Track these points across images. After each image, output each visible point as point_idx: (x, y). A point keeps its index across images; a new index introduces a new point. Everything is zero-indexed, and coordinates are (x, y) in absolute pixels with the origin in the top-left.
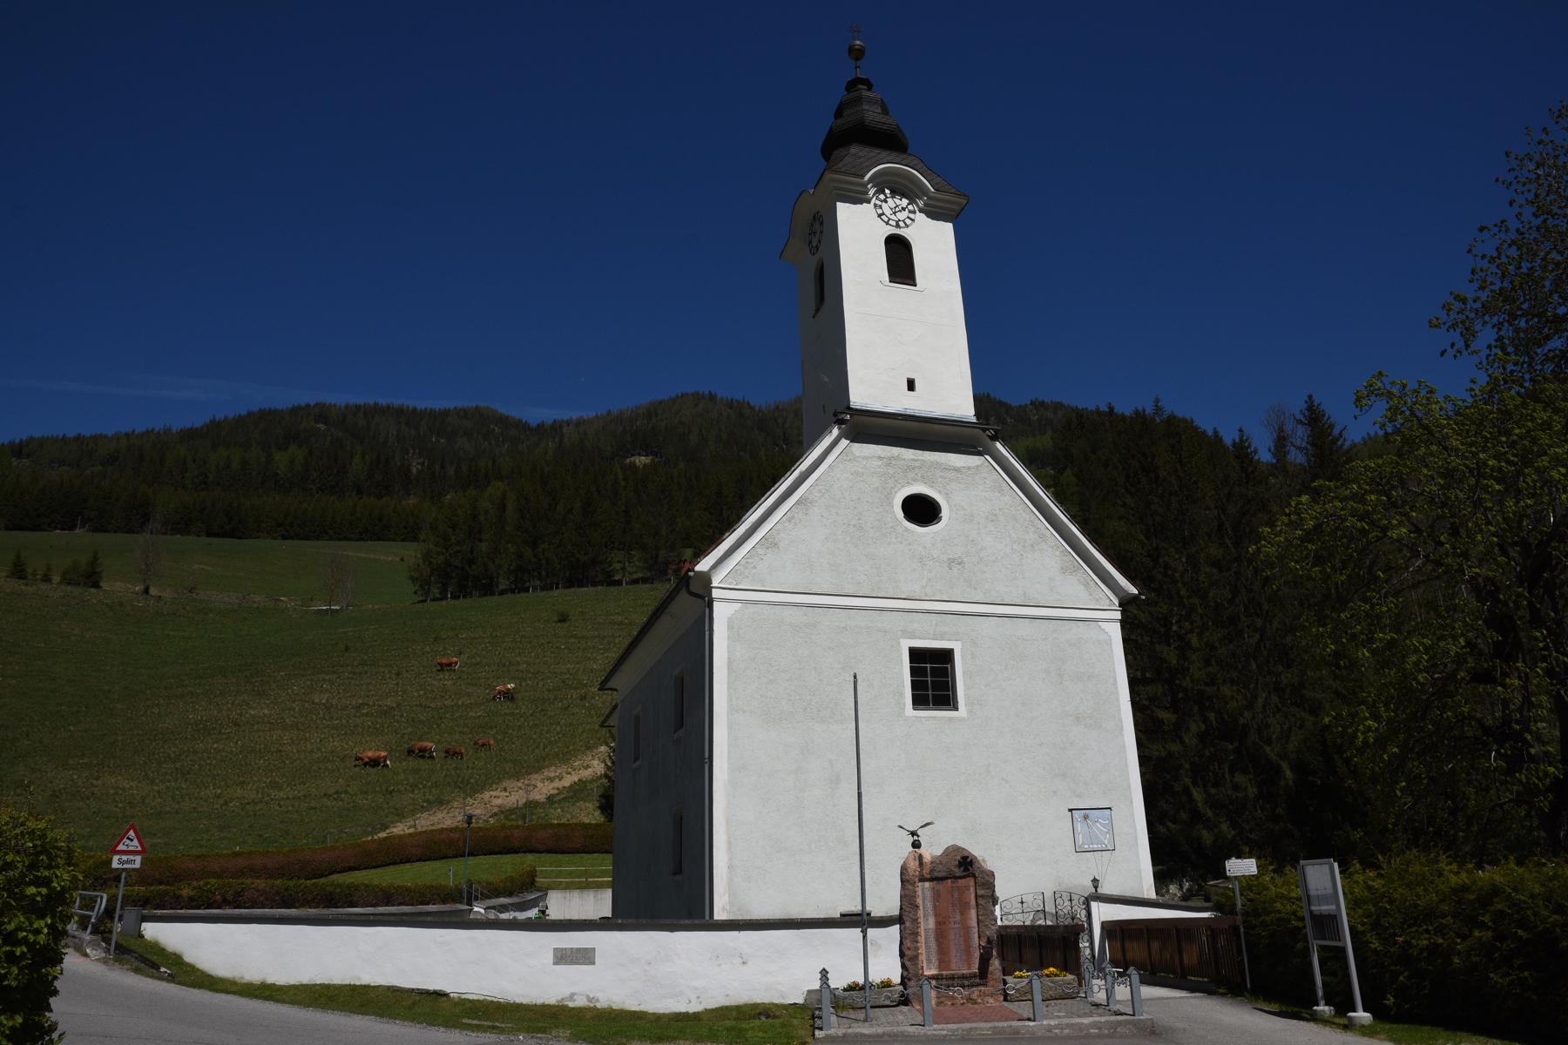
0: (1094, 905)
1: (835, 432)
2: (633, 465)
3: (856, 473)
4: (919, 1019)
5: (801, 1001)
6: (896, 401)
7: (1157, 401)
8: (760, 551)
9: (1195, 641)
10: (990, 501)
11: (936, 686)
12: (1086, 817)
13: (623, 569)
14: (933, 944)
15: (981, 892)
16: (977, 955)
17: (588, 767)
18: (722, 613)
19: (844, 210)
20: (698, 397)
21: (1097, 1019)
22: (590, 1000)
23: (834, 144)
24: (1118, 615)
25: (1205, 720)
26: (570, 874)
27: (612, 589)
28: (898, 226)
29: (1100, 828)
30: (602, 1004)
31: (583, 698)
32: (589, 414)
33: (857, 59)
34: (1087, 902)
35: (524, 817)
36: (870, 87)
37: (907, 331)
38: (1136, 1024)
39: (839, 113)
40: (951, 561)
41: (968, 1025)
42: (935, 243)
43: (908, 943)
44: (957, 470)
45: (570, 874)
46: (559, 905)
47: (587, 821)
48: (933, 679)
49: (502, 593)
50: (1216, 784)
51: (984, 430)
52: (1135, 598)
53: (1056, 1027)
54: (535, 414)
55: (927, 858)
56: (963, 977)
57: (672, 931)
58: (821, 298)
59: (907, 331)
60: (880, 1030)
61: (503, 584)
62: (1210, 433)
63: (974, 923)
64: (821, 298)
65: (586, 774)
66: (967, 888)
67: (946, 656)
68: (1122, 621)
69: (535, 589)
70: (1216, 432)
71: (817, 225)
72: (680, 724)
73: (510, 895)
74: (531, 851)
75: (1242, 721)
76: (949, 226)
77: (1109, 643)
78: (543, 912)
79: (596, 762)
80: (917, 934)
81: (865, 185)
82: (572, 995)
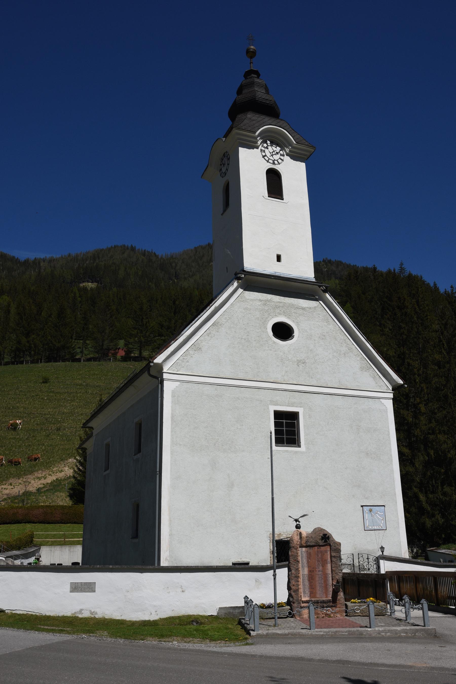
0: (381, 562)
1: (236, 284)
2: (85, 289)
3: (246, 309)
4: (305, 626)
5: (215, 614)
6: (270, 267)
7: (402, 264)
8: (191, 352)
9: (423, 409)
10: (320, 326)
11: (288, 433)
12: (371, 511)
13: (82, 352)
14: (307, 583)
15: (333, 554)
16: (331, 589)
17: (62, 471)
18: (169, 388)
19: (243, 152)
20: (124, 248)
21: (405, 628)
22: (92, 613)
23: (236, 111)
24: (391, 396)
25: (428, 455)
26: (54, 536)
27: (75, 364)
28: (274, 163)
29: (378, 516)
30: (99, 615)
31: (58, 429)
32: (56, 256)
33: (251, 58)
34: (377, 560)
35: (23, 501)
36: (258, 75)
37: (277, 228)
38: (426, 631)
39: (239, 92)
40: (299, 362)
41: (335, 630)
42: (295, 175)
43: (293, 582)
44: (303, 309)
45: (54, 536)
46: (48, 555)
47: (61, 504)
48: (287, 428)
49: (7, 364)
50: (433, 492)
51: (320, 286)
52: (402, 386)
53: (383, 631)
54: (23, 255)
55: (304, 534)
56: (323, 602)
57: (142, 572)
58: (227, 204)
59: (277, 228)
60: (287, 632)
61: (7, 359)
62: (432, 285)
63: (329, 571)
64: (227, 204)
65: (61, 475)
66: (326, 551)
67: (294, 416)
68: (393, 399)
69: (27, 362)
70: (435, 284)
71: (225, 159)
72: (139, 450)
73: (19, 549)
74: (29, 522)
75: (449, 455)
76: (303, 165)
77: (386, 411)
78: (38, 559)
79: (67, 468)
80: (298, 577)
81: (256, 138)
82: (81, 610)
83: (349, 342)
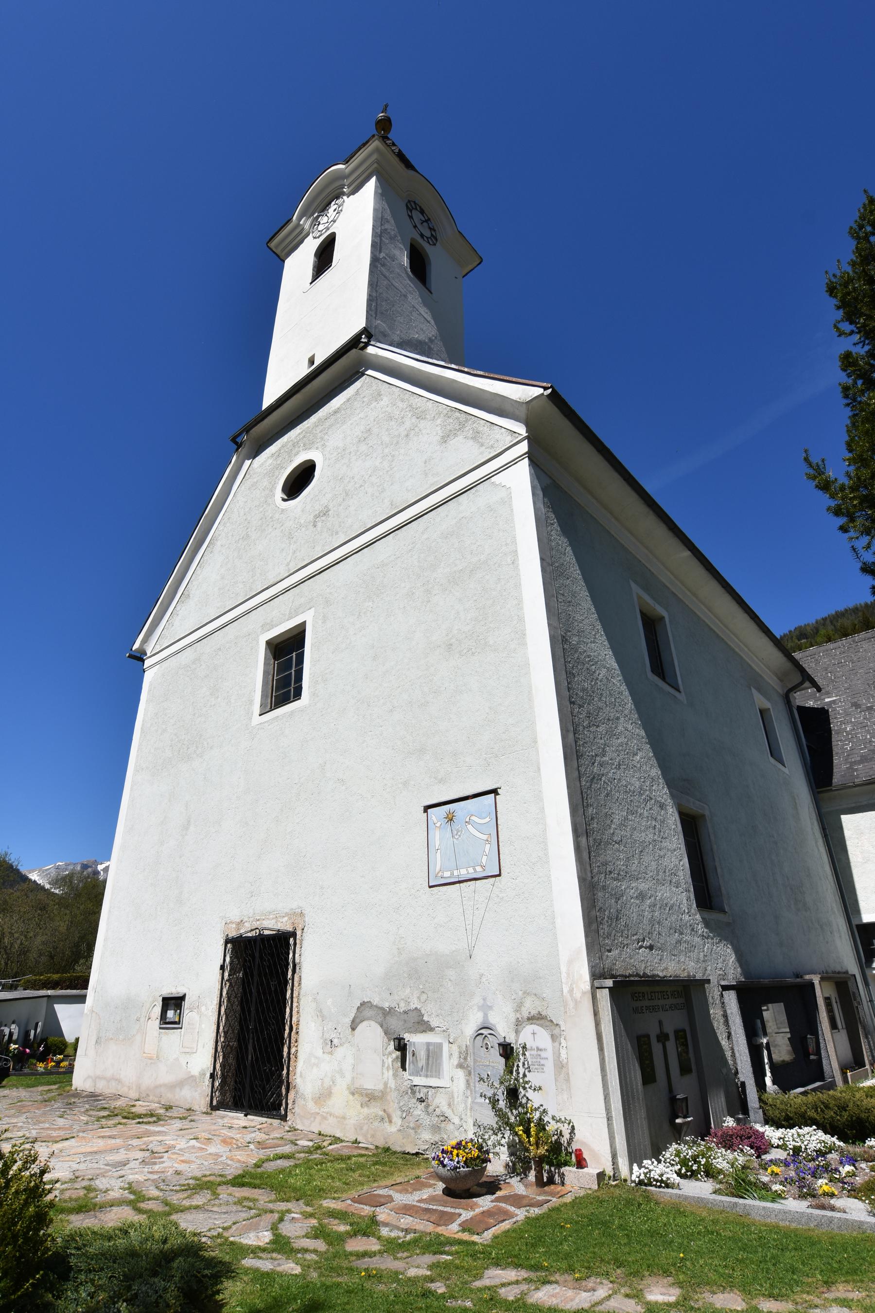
81: (298, 225)
83: (416, 401)
